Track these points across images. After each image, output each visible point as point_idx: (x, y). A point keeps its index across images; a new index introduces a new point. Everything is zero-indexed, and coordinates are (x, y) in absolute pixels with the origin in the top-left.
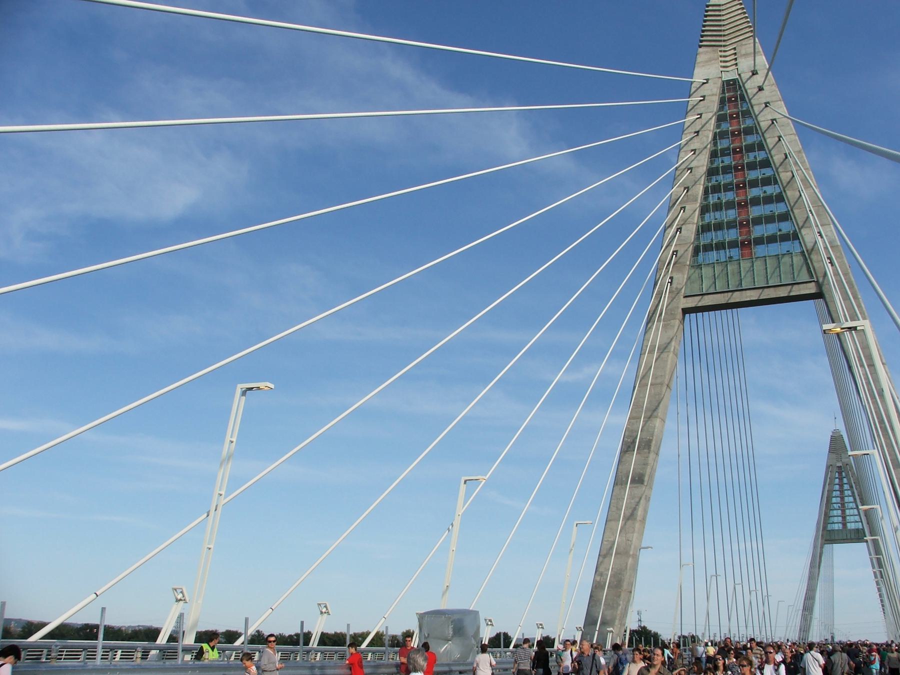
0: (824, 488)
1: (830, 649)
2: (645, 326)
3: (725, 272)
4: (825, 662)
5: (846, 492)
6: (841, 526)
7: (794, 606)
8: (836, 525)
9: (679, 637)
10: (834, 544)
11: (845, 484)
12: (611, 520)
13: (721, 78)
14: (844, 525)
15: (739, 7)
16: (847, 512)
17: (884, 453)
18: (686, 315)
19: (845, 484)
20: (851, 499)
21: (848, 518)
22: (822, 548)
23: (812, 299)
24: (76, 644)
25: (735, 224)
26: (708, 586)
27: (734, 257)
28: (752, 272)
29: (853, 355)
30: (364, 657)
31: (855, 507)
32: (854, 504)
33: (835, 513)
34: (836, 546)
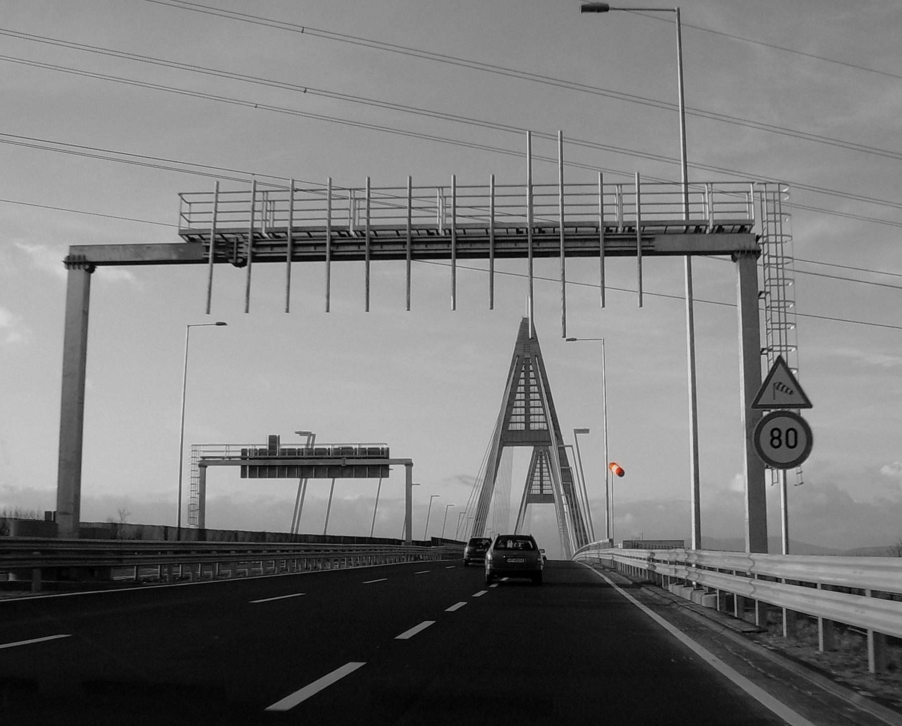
0: (510, 376)
1: (113, 576)
2: (121, 571)
3: (389, 557)
4: (490, 573)
5: (531, 380)
6: (539, 491)
7: (465, 513)
8: (518, 417)
9: (877, 679)
10: (515, 447)
11: (532, 378)
12: (190, 206)
14: (527, 423)
15: (481, 478)
16: (544, 478)
17: (556, 425)
18: (534, 221)
19: (532, 378)
20: (547, 474)
21: (544, 487)
22: (500, 450)
23: (757, 268)
24: (46, 593)
25: (342, 541)
26: (384, 206)
27: (657, 568)
28: (230, 447)
29: (28, 542)
30: (634, 574)
31: (541, 405)
33: (518, 403)
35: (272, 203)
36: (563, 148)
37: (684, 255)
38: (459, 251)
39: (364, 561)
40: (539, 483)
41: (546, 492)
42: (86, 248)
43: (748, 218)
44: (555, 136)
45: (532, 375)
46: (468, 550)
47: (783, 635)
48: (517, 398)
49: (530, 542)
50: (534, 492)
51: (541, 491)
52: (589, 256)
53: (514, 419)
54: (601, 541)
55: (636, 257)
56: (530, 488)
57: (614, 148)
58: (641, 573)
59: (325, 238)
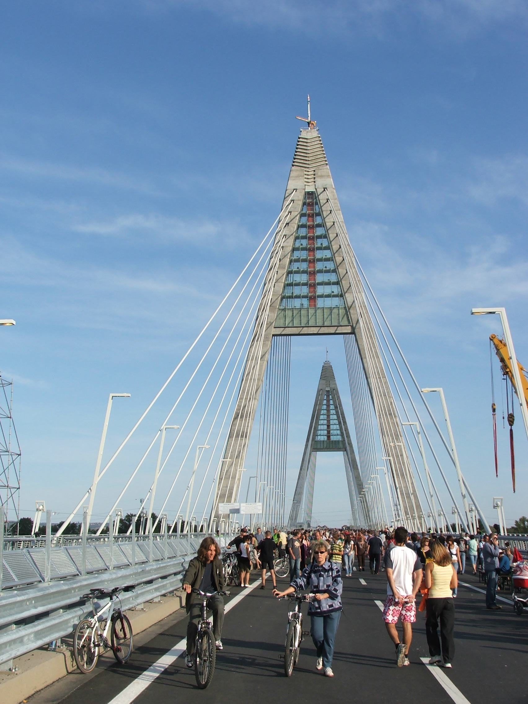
6: (326, 438)
13: (305, 189)
18: (486, 592)
32: (338, 426)
34: (319, 453)
35: (174, 537)
36: (343, 332)
37: (364, 562)
38: (103, 659)
39: (93, 620)
40: (325, 422)
41: (339, 215)
42: (314, 474)
43: (485, 592)
44: (415, 632)
45: (331, 402)
46: (312, 579)
47: (396, 663)
48: (321, 419)
49: (371, 487)
50: (319, 438)
51: (329, 437)
52: (312, 415)
53: (319, 432)
54: (75, 690)
55: (337, 324)
56: (315, 435)
57: (285, 581)
58: (42, 543)
59: (334, 657)
